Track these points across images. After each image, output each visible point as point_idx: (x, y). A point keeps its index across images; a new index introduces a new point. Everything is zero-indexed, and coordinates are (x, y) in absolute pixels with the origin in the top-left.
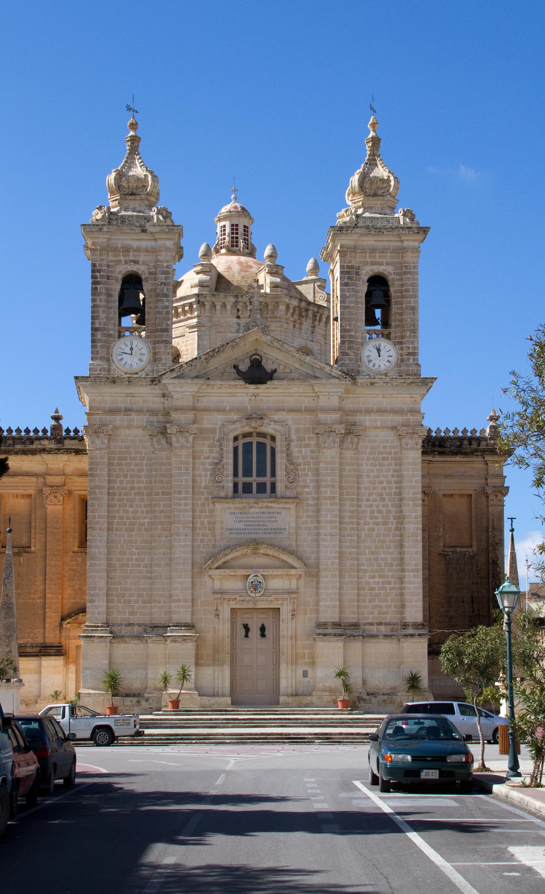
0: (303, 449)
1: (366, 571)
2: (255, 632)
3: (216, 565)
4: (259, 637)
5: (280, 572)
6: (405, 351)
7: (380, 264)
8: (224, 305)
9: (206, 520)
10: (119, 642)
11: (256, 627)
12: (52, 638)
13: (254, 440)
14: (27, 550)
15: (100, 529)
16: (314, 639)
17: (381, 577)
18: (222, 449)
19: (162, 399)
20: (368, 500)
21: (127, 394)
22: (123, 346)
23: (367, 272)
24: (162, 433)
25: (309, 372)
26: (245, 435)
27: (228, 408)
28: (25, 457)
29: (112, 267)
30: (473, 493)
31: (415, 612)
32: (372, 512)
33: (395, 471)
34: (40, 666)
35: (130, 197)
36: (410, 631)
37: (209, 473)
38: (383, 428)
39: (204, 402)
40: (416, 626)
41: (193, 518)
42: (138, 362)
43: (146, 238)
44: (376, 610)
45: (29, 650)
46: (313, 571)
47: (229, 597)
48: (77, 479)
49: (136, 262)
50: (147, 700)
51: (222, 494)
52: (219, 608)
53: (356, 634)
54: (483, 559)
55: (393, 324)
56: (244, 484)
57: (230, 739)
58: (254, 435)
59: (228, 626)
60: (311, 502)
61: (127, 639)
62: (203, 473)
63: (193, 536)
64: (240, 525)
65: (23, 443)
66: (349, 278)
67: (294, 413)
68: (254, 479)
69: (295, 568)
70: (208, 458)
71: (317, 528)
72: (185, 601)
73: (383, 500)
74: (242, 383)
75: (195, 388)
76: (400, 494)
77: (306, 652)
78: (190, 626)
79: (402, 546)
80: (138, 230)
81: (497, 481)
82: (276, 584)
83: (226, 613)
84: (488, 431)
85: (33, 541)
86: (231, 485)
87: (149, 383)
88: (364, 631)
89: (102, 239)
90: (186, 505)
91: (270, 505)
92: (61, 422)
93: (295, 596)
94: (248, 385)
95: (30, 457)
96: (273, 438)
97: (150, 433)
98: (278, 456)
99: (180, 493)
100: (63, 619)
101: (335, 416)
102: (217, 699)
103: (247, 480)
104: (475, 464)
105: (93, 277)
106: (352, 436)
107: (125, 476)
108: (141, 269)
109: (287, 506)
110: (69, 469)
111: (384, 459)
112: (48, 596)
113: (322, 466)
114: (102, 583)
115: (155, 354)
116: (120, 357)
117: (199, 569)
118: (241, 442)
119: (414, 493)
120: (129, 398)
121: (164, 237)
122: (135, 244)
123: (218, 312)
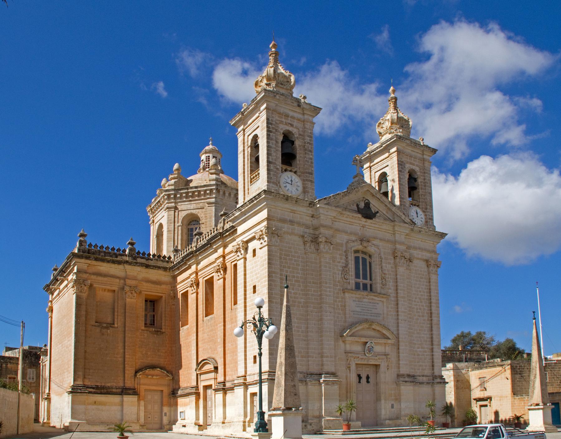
2: (364, 380)
7: (413, 164)
8: (230, 194)
9: (339, 304)
11: (367, 376)
12: (129, 384)
14: (112, 325)
15: (276, 303)
17: (422, 348)
21: (292, 210)
22: (286, 178)
25: (391, 218)
27: (349, 232)
28: (113, 265)
29: (278, 124)
34: (122, 401)
35: (281, 86)
37: (340, 272)
38: (421, 259)
39: (337, 225)
42: (296, 191)
43: (298, 111)
44: (421, 368)
45: (114, 390)
48: (144, 284)
49: (292, 125)
50: (311, 425)
62: (337, 272)
64: (358, 309)
65: (111, 256)
68: (361, 281)
69: (389, 339)
70: (339, 262)
72: (331, 357)
73: (421, 302)
75: (334, 214)
78: (333, 374)
82: (378, 349)
85: (116, 320)
87: (308, 205)
90: (330, 292)
92: (134, 246)
95: (116, 266)
99: (326, 283)
100: (136, 372)
107: (289, 267)
109: (382, 299)
110: (140, 277)
112: (126, 356)
115: (304, 188)
116: (285, 185)
120: (292, 214)
121: (309, 113)
122: (291, 114)
123: (226, 197)
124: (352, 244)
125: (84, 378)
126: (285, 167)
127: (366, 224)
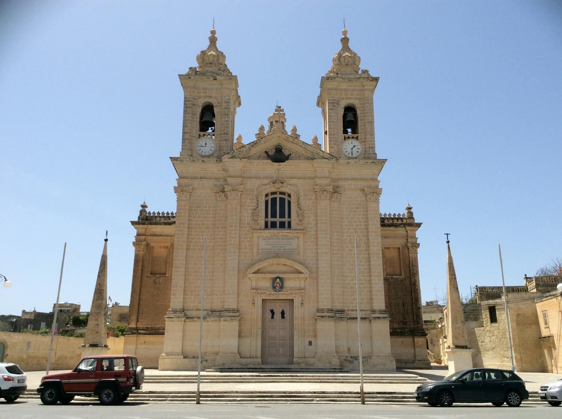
0: (308, 202)
1: (348, 276)
2: (278, 315)
3: (253, 271)
4: (281, 318)
5: (294, 276)
6: (367, 146)
10: (190, 321)
13: (278, 196)
16: (316, 319)
18: (258, 201)
19: (223, 172)
20: (348, 233)
23: (344, 103)
24: (223, 192)
26: (273, 193)
30: (400, 247)
31: (380, 303)
32: (351, 240)
33: (364, 215)
35: (209, 65)
36: (377, 315)
37: (250, 215)
40: (381, 312)
41: (240, 242)
46: (315, 275)
47: (261, 291)
49: (210, 97)
50: (206, 361)
51: (258, 227)
52: (255, 299)
53: (343, 316)
54: (408, 282)
55: (360, 131)
56: (272, 223)
57: (242, 397)
58: (278, 193)
59: (260, 310)
60: (313, 233)
61: (196, 319)
63: (239, 253)
66: (333, 106)
67: (301, 180)
68: (278, 220)
70: (249, 206)
71: (317, 249)
73: (357, 232)
74: (270, 161)
76: (367, 229)
77: (311, 328)
79: (369, 261)
80: (212, 79)
81: (414, 240)
83: (259, 303)
84: (406, 215)
86: (263, 222)
88: (347, 315)
89: (191, 83)
91: (287, 234)
93: (303, 291)
94: (274, 163)
96: (289, 196)
97: (215, 191)
98: (292, 205)
99: (231, 226)
101: (327, 181)
102: (252, 360)
103: (274, 220)
104: (401, 231)
105: (185, 104)
106: (337, 194)
107: (199, 217)
108: (214, 101)
111: (357, 208)
113: (319, 211)
114: (181, 283)
117: (241, 273)
118: (270, 197)
119: (376, 228)
124: (264, 187)
125: (137, 321)
126: (202, 133)
127: (280, 167)
